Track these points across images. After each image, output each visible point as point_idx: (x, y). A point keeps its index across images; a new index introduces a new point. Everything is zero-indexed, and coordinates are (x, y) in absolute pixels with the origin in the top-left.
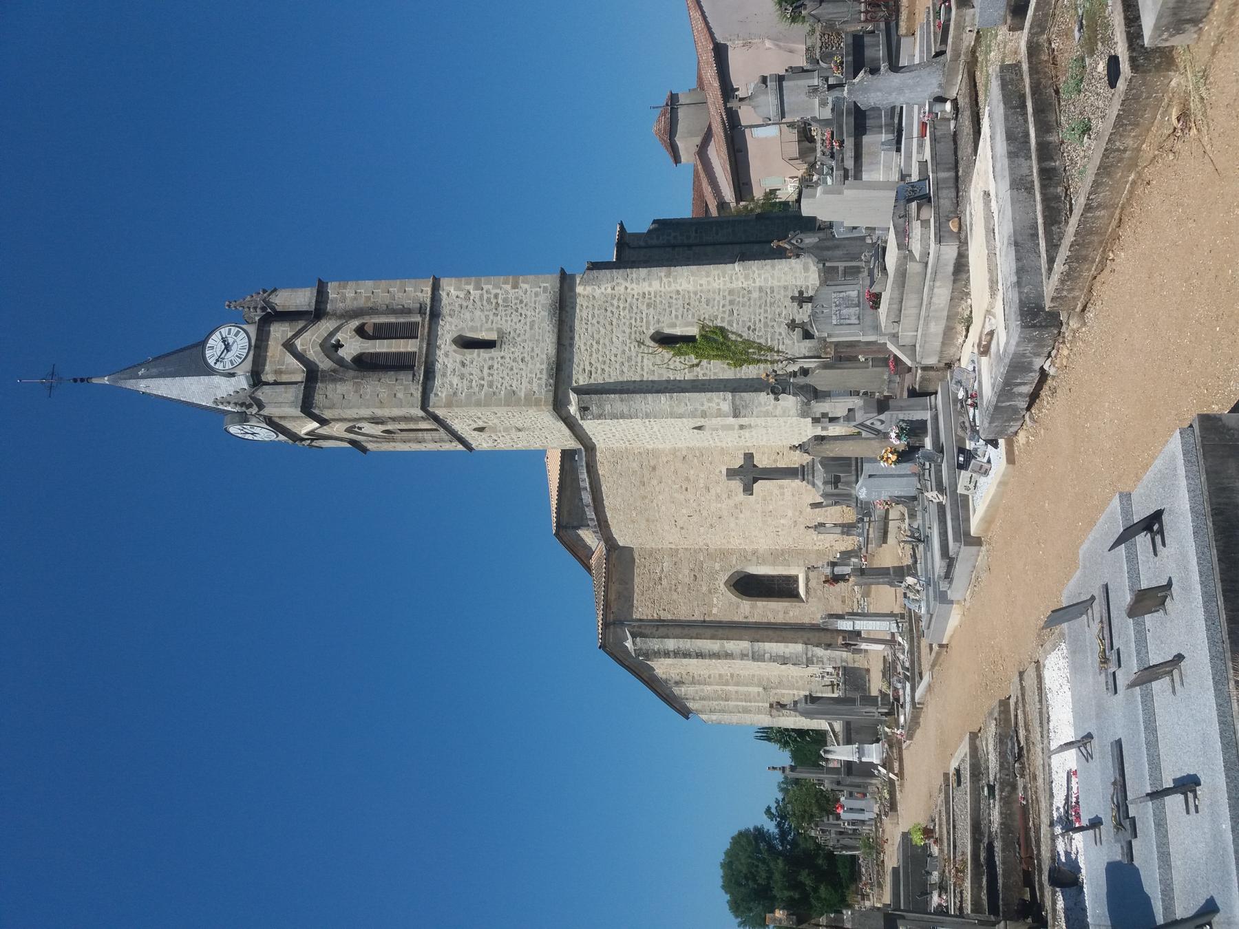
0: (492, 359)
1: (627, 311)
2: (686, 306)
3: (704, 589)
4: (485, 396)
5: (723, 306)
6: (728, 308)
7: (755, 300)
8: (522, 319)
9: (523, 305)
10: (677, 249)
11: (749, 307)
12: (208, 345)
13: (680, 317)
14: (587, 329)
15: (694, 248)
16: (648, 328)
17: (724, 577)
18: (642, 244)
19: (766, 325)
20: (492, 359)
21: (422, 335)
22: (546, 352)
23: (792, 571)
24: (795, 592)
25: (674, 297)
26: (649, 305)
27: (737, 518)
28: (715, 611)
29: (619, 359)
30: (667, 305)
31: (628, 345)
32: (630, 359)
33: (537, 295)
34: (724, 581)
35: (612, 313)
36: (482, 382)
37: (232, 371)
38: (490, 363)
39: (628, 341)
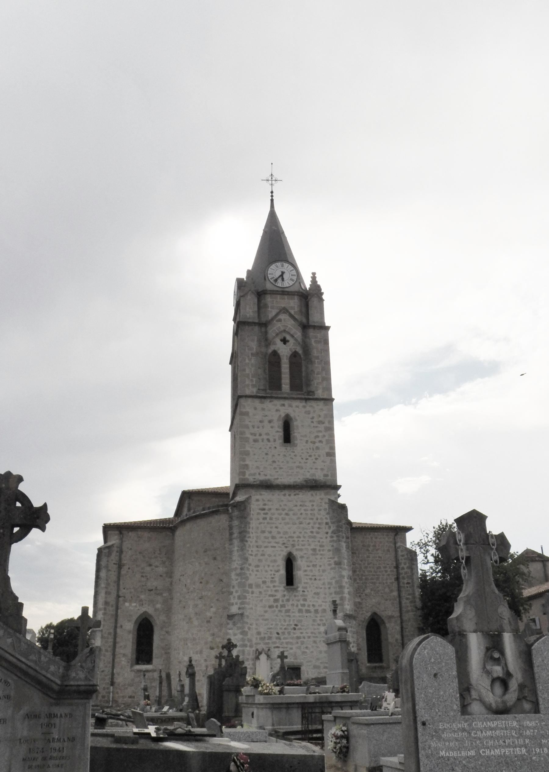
0: (275, 441)
1: (310, 534)
2: (313, 578)
3: (143, 597)
4: (247, 437)
5: (313, 605)
6: (312, 609)
7: (318, 629)
8: (304, 460)
9: (314, 460)
10: (395, 570)
11: (312, 625)
12: (284, 264)
13: (306, 573)
14: (296, 506)
15: (396, 582)
16: (297, 550)
17: (150, 610)
18: (399, 544)
19: (298, 638)
20: (275, 441)
21: (292, 394)
22: (280, 477)
23: (155, 661)
24: (140, 662)
25: (321, 569)
26: (314, 550)
27: (184, 619)
28: (127, 604)
29: (274, 530)
30: (315, 563)
31: (284, 536)
32: (273, 537)
33: (322, 469)
34: (147, 610)
35: (309, 524)
36: (258, 435)
37: (267, 278)
38: (271, 440)
39: (287, 536)
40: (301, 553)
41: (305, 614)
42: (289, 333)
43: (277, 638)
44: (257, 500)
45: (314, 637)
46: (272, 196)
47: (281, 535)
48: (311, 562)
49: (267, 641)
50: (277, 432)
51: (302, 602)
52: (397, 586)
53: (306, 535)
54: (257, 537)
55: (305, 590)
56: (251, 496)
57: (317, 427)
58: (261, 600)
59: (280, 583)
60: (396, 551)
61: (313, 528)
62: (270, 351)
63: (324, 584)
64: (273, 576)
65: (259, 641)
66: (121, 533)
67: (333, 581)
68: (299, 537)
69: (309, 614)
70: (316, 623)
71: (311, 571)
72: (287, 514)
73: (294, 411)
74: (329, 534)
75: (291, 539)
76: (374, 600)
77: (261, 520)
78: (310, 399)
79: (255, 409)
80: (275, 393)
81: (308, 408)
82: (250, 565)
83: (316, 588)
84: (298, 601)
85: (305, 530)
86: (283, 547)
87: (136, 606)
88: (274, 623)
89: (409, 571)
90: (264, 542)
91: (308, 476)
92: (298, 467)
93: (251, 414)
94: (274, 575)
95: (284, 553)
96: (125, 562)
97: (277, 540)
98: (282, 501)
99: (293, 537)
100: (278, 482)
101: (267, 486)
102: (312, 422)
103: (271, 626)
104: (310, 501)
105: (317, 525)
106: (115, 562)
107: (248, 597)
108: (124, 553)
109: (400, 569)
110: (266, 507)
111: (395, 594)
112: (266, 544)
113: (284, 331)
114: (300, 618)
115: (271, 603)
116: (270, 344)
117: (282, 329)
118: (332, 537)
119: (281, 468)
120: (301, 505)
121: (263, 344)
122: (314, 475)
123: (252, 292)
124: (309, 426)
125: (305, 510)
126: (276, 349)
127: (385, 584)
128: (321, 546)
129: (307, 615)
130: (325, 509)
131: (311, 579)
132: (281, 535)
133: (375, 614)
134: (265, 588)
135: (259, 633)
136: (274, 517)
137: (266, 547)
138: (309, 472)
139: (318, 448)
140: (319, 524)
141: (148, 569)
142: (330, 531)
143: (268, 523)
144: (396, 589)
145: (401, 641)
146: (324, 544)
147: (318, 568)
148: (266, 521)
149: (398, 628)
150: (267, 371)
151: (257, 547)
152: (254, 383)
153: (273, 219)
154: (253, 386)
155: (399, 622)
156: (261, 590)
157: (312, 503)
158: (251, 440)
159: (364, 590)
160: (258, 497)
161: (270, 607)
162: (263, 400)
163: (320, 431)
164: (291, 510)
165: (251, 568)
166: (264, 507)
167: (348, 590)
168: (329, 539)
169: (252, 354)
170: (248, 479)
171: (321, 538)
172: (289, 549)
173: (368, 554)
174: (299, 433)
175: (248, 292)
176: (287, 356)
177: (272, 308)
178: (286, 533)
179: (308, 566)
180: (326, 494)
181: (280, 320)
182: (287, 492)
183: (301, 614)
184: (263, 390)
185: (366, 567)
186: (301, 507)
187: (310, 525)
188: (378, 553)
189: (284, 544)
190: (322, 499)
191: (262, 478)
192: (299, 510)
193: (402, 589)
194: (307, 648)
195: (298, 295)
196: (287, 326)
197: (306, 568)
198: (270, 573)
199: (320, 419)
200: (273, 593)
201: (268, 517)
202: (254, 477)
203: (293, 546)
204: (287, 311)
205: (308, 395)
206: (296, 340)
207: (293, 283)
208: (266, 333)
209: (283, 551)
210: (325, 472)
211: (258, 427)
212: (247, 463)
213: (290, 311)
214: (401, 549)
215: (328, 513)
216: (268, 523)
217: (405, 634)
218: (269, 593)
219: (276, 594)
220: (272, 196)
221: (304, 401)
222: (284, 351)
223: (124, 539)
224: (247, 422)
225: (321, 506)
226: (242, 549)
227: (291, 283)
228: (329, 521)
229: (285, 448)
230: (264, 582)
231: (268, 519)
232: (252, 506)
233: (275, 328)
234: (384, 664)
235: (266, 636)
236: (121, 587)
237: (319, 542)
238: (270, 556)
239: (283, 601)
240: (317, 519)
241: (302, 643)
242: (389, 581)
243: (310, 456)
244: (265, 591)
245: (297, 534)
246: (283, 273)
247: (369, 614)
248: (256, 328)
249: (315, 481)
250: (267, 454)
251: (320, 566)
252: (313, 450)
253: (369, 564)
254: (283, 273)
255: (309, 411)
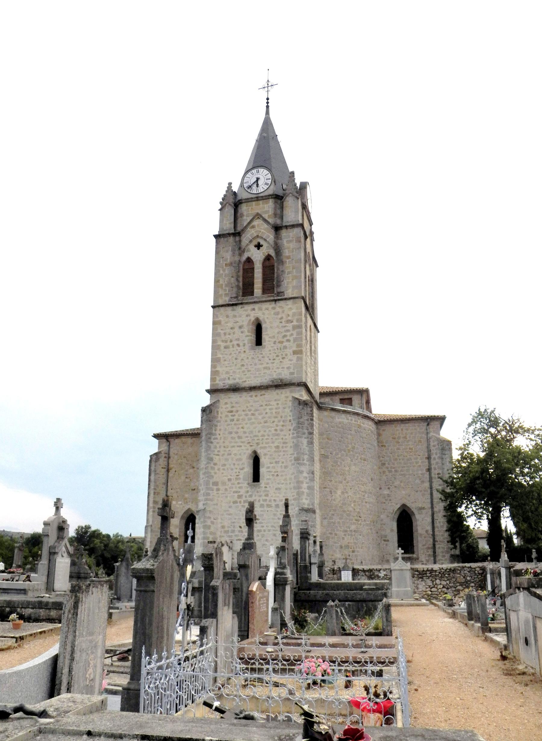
0: (244, 345)
2: (276, 474)
3: (187, 496)
4: (218, 345)
6: (273, 504)
10: (427, 460)
12: (260, 169)
13: (268, 470)
14: (262, 406)
15: (428, 473)
16: (261, 448)
20: (244, 345)
26: (277, 447)
30: (278, 460)
32: (239, 437)
34: (191, 507)
35: (273, 422)
38: (241, 344)
40: (265, 451)
41: (266, 509)
42: (262, 238)
43: (239, 531)
44: (226, 403)
45: (274, 530)
46: (268, 103)
47: (247, 435)
48: (274, 459)
49: (230, 534)
50: (247, 336)
51: (265, 498)
52: (428, 476)
53: (270, 433)
54: (225, 438)
55: (267, 486)
56: (219, 401)
57: (285, 326)
58: (227, 497)
59: (244, 480)
60: (428, 440)
61: (277, 426)
62: (244, 258)
63: (285, 480)
64: (237, 474)
65: (223, 534)
66: (168, 441)
67: (293, 477)
68: (263, 436)
69: (270, 509)
70: (276, 518)
71: (274, 467)
72: (253, 414)
73: (264, 314)
74: (292, 431)
75: (256, 438)
76: (404, 492)
77: (229, 422)
78: (279, 300)
79: (227, 316)
80: (249, 299)
81: (278, 309)
82: (215, 464)
83: (278, 484)
84: (260, 496)
85: (270, 429)
86: (248, 445)
87: (181, 504)
88: (237, 517)
89: (439, 461)
90: (230, 442)
91: (275, 376)
92: (265, 368)
93: (223, 323)
94: (239, 472)
95: (250, 451)
96: (172, 466)
97: (242, 440)
98: (249, 402)
99: (257, 436)
100: (247, 384)
101: (235, 389)
102: (281, 322)
103: (234, 521)
104: (276, 400)
105: (282, 423)
106: (164, 467)
107: (212, 494)
108: (172, 458)
109: (432, 459)
110: (234, 409)
111: (427, 485)
112: (233, 444)
113: (258, 236)
114: (262, 513)
115: (236, 498)
116: (244, 252)
117: (255, 235)
118: (293, 434)
119: (248, 371)
120: (266, 405)
121: (237, 252)
122: (280, 374)
123: (230, 204)
124: (278, 327)
125: (270, 409)
126: (250, 256)
127: (416, 476)
128: (284, 443)
129: (268, 509)
130: (289, 407)
131: (273, 475)
132: (247, 435)
133: (404, 505)
134: (230, 485)
135: (223, 527)
136: (241, 418)
137: (233, 447)
138: (275, 372)
139: (285, 347)
140: (283, 421)
141: (191, 471)
142: (292, 428)
143: (235, 424)
144: (428, 479)
145: (432, 533)
146: (287, 441)
147: (280, 464)
148: (233, 423)
149: (429, 519)
150: (241, 279)
151: (224, 447)
152: (227, 292)
153: (267, 125)
154: (226, 295)
155: (430, 513)
156: (227, 487)
157: (276, 402)
158: (222, 348)
159: (393, 483)
160: (226, 401)
161: (235, 502)
162: (235, 307)
163: (288, 331)
164: (256, 410)
165: (216, 467)
166: (232, 409)
167: (307, 485)
168: (291, 436)
169: (226, 265)
170: (218, 384)
171: (285, 435)
172: (253, 448)
173: (397, 446)
174: (267, 335)
175: (226, 205)
176: (259, 260)
177: (247, 216)
178: (251, 432)
179: (271, 463)
180: (291, 392)
181: (253, 227)
182: (253, 393)
183: (262, 509)
184: (235, 298)
185: (396, 459)
186: (266, 407)
187: (275, 423)
188: (409, 445)
189: (249, 443)
190: (287, 397)
191: (231, 382)
192: (265, 409)
193: (433, 480)
194: (267, 540)
195: (272, 198)
196: (260, 231)
197: (269, 465)
198: (235, 471)
199: (290, 318)
200: (238, 490)
201: (235, 418)
202: (224, 382)
203: (258, 444)
204: (261, 216)
205: (278, 296)
206: (268, 243)
207: (268, 187)
208: (240, 241)
209: (247, 449)
210: (292, 370)
211: (229, 334)
212: (217, 369)
213: (263, 216)
214: (433, 439)
215: (291, 411)
216: (235, 424)
217: (435, 525)
218: (234, 490)
219: (240, 490)
220: (268, 103)
221: (274, 302)
222: (258, 256)
223: (171, 446)
224: (219, 331)
225: (286, 404)
226: (208, 448)
227: (266, 187)
228: (291, 418)
229: (253, 351)
230: (229, 480)
231: (235, 420)
232: (220, 409)
233: (248, 235)
234: (415, 556)
235: (230, 529)
236: (169, 488)
237: (282, 439)
238: (235, 454)
239: (246, 497)
240: (281, 417)
241: (263, 536)
242: (420, 472)
243: (277, 356)
244: (230, 488)
245: (262, 433)
246: (258, 179)
247: (398, 506)
248: (231, 239)
249: (281, 380)
250: (236, 359)
251: (283, 463)
252: (281, 349)
253: (398, 456)
254: (258, 179)
255: (278, 312)
